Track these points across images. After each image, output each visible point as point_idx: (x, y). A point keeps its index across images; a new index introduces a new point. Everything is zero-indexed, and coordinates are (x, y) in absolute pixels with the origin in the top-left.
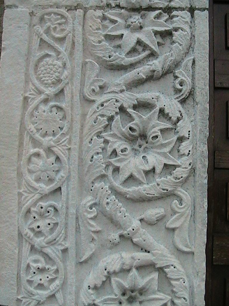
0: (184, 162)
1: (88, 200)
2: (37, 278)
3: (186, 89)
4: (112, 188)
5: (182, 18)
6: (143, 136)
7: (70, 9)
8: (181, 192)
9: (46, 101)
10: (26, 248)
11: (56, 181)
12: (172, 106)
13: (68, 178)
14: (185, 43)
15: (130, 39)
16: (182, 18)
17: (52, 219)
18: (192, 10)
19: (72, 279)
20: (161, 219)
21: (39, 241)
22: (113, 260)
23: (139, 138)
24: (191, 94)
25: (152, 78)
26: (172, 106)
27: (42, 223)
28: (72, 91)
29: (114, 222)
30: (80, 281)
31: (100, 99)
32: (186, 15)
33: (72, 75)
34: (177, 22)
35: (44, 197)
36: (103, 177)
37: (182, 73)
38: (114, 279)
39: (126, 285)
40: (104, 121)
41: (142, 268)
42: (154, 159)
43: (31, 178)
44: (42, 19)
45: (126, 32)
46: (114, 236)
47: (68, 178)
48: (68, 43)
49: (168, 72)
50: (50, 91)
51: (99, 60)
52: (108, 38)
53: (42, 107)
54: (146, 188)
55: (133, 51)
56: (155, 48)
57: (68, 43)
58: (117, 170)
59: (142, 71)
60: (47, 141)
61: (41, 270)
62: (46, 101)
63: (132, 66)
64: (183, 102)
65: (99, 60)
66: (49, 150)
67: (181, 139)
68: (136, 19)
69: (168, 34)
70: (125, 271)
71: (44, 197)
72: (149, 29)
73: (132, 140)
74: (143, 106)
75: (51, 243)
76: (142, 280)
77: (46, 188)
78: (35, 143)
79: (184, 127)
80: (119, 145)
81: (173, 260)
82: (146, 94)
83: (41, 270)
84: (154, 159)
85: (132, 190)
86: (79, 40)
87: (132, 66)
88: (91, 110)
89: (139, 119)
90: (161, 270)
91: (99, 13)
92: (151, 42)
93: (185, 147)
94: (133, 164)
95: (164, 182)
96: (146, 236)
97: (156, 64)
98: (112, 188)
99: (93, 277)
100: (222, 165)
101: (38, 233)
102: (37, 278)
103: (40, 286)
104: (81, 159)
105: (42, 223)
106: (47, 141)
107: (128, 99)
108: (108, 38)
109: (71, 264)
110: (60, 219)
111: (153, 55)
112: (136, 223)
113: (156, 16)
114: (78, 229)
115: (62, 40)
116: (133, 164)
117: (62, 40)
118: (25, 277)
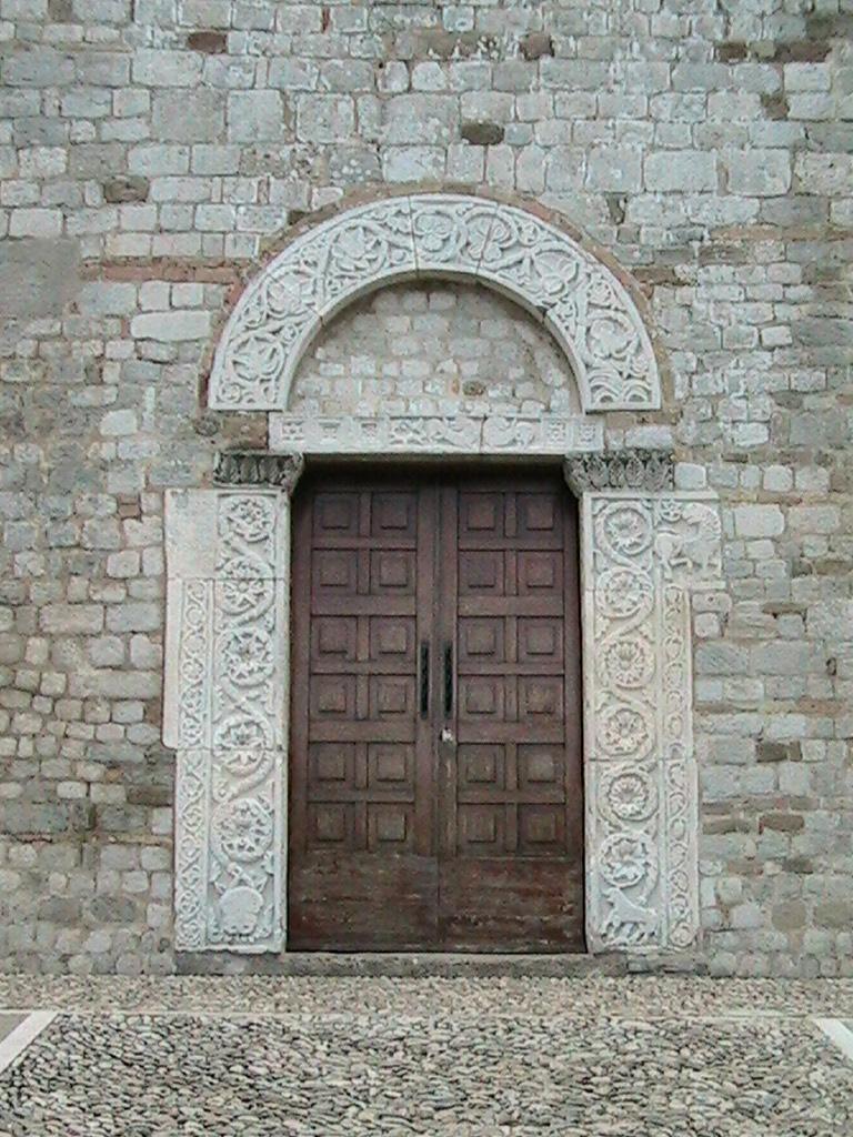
1: (218, 687)
2: (189, 732)
3: (270, 626)
4: (232, 682)
7: (206, 580)
8: (267, 681)
9: (194, 633)
10: (183, 715)
11: (48, 893)
12: (263, 635)
13: (206, 677)
15: (240, 597)
18: (275, 580)
19: (209, 731)
20: (258, 696)
21: (190, 711)
22: (232, 721)
23: (245, 653)
25: (252, 619)
26: (263, 635)
28: (208, 628)
29: (234, 701)
30: (213, 733)
31: (223, 632)
32: (271, 583)
34: (266, 588)
35: (193, 686)
36: (225, 675)
37: (266, 862)
38: (232, 731)
39: (239, 733)
40: (225, 644)
41: (248, 724)
42: (254, 664)
43: (186, 676)
44: (190, 587)
45: (237, 594)
46: (232, 707)
47: (206, 677)
49: (261, 615)
50: (196, 628)
51: (224, 611)
52: (228, 598)
53: (193, 637)
54: (249, 680)
55: (241, 605)
56: (254, 603)
58: (233, 671)
59: (246, 616)
60: (195, 655)
61: (192, 727)
62: (194, 633)
63: (241, 613)
64: (270, 632)
65: (224, 611)
66: (196, 661)
67: (267, 653)
68: (243, 585)
69: (261, 594)
70: (238, 726)
71: (193, 686)
72: (251, 591)
73: (241, 654)
74: (247, 635)
75: (198, 711)
76: (244, 730)
77: (195, 682)
78: (188, 657)
79: (269, 647)
80: (234, 657)
81: (264, 719)
82: (248, 629)
83: (192, 727)
84: (254, 664)
85: (241, 682)
87: (241, 613)
90: (258, 725)
92: (252, 600)
93: (270, 657)
94: (242, 667)
95: (259, 677)
96: (249, 706)
97: (254, 612)
99: (221, 730)
101: (190, 706)
102: (189, 732)
103: (192, 736)
105: (194, 702)
106: (195, 655)
107: (239, 632)
108: (228, 598)
110: (202, 698)
111: (253, 606)
112: (244, 699)
113: (586, 457)
115: (201, 599)
116: (242, 667)
117: (201, 599)
118: (183, 731)
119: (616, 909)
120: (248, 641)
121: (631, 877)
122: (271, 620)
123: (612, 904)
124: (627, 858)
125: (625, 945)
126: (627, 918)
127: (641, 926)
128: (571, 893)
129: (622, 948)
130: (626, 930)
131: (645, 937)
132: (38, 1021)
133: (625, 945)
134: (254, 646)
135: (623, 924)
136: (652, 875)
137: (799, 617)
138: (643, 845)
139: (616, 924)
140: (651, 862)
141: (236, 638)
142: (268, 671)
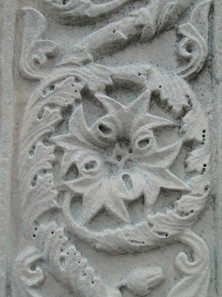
1: (29, 253)
3: (198, 57)
8: (191, 237)
12: (174, 87)
23: (116, 144)
25: (137, 39)
26: (174, 87)
31: (49, 77)
40: (56, 115)
42: (143, 180)
54: (129, 231)
58: (78, 200)
59: (120, 27)
64: (193, 79)
73: (103, 146)
74: (122, 87)
80: (80, 156)
82: (127, 67)
84: (143, 180)
85: (104, 234)
93: (197, 158)
95: (161, 220)
116: (107, 188)
120: (127, 104)
122: (201, 41)
128: (81, 200)
132: (96, 138)
134: (147, 122)
137: (217, 181)
141: (86, 94)
142: (190, 203)
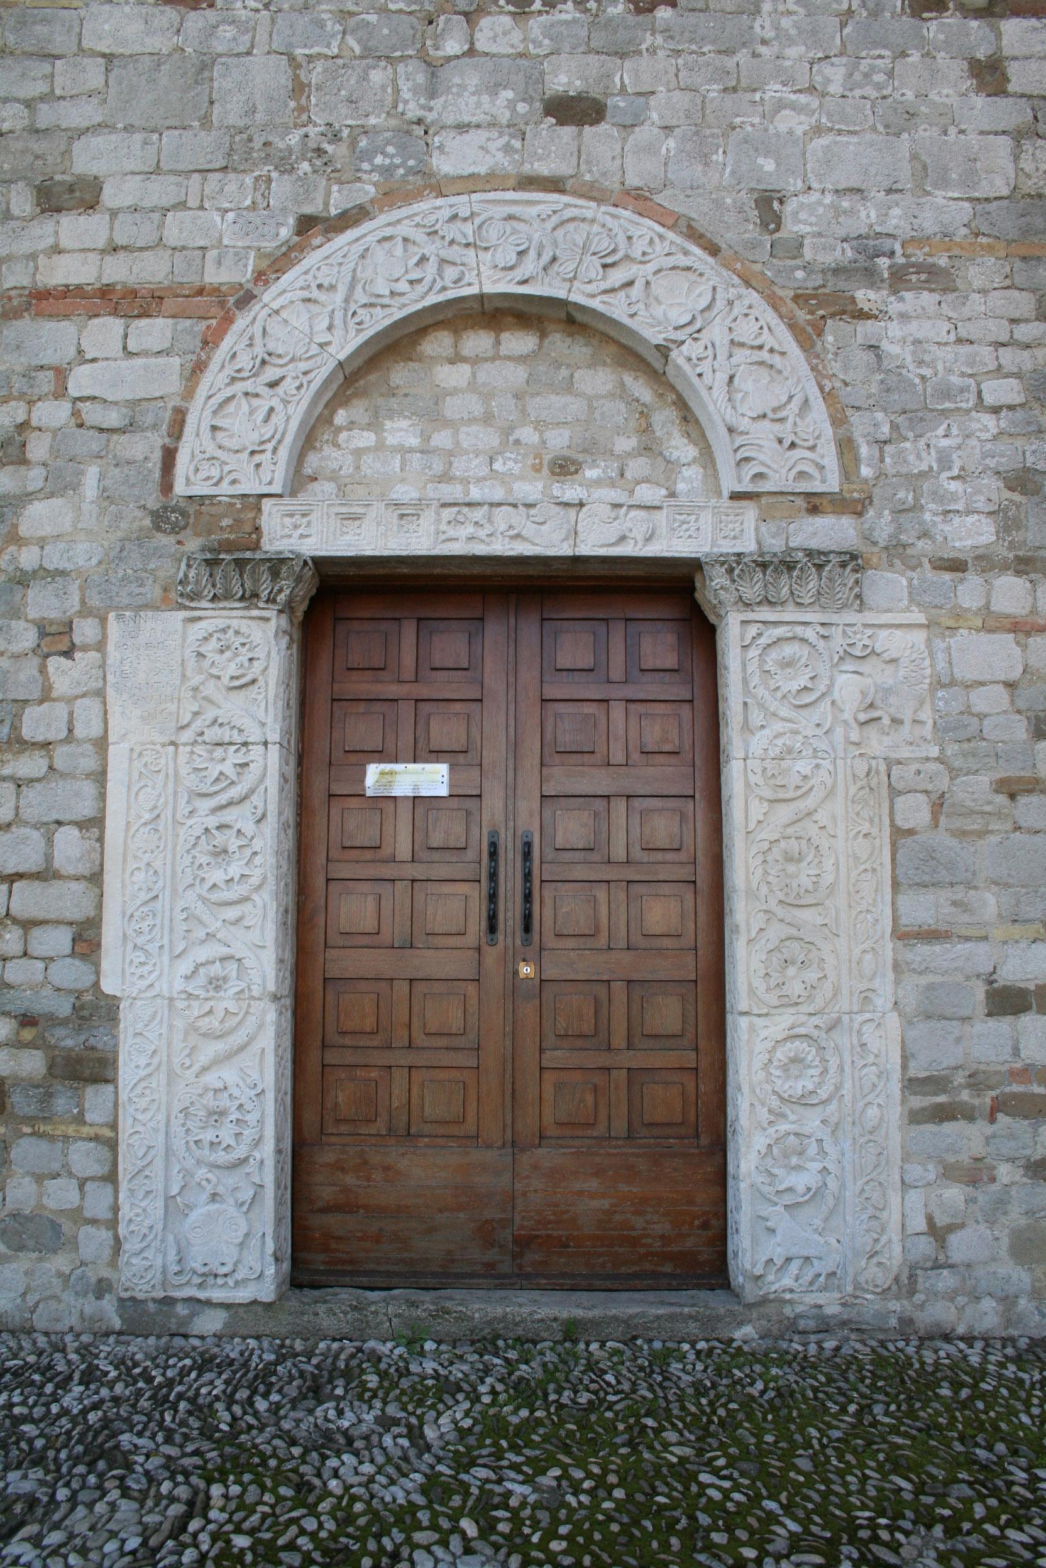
0: (257, 872)
3: (259, 812)
5: (257, 751)
6: (225, 851)
8: (255, 897)
14: (259, 772)
16: (257, 751)
17: (149, 921)
18: (266, 744)
22: (203, 954)
24: (264, 816)
26: (249, 828)
27: (144, 926)
31: (190, 822)
32: (261, 748)
33: (166, 803)
42: (235, 870)
48: (162, 776)
50: (147, 816)
57: (162, 776)
59: (223, 799)
61: (142, 964)
73: (216, 854)
79: (257, 845)
80: (204, 859)
83: (142, 964)
85: (215, 896)
86: (171, 772)
88: (830, 339)
89: (220, 838)
91: (188, 749)
92: (230, 772)
93: (258, 860)
94: (217, 876)
97: (234, 792)
98: (200, 896)
100: (906, 826)
104: (174, 871)
107: (212, 822)
109: (166, 958)
114: (171, 930)
116: (217, 876)
119: (778, 1239)
121: (801, 1189)
123: (772, 1231)
124: (794, 1161)
125: (791, 1291)
126: (794, 1251)
127: (815, 1262)
129: (788, 1296)
130: (794, 1268)
131: (822, 1279)
133: (791, 1291)
135: (789, 1260)
136: (832, 1184)
138: (820, 1141)
139: (779, 1262)
140: (831, 1167)
